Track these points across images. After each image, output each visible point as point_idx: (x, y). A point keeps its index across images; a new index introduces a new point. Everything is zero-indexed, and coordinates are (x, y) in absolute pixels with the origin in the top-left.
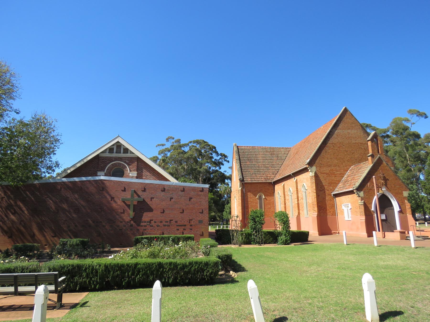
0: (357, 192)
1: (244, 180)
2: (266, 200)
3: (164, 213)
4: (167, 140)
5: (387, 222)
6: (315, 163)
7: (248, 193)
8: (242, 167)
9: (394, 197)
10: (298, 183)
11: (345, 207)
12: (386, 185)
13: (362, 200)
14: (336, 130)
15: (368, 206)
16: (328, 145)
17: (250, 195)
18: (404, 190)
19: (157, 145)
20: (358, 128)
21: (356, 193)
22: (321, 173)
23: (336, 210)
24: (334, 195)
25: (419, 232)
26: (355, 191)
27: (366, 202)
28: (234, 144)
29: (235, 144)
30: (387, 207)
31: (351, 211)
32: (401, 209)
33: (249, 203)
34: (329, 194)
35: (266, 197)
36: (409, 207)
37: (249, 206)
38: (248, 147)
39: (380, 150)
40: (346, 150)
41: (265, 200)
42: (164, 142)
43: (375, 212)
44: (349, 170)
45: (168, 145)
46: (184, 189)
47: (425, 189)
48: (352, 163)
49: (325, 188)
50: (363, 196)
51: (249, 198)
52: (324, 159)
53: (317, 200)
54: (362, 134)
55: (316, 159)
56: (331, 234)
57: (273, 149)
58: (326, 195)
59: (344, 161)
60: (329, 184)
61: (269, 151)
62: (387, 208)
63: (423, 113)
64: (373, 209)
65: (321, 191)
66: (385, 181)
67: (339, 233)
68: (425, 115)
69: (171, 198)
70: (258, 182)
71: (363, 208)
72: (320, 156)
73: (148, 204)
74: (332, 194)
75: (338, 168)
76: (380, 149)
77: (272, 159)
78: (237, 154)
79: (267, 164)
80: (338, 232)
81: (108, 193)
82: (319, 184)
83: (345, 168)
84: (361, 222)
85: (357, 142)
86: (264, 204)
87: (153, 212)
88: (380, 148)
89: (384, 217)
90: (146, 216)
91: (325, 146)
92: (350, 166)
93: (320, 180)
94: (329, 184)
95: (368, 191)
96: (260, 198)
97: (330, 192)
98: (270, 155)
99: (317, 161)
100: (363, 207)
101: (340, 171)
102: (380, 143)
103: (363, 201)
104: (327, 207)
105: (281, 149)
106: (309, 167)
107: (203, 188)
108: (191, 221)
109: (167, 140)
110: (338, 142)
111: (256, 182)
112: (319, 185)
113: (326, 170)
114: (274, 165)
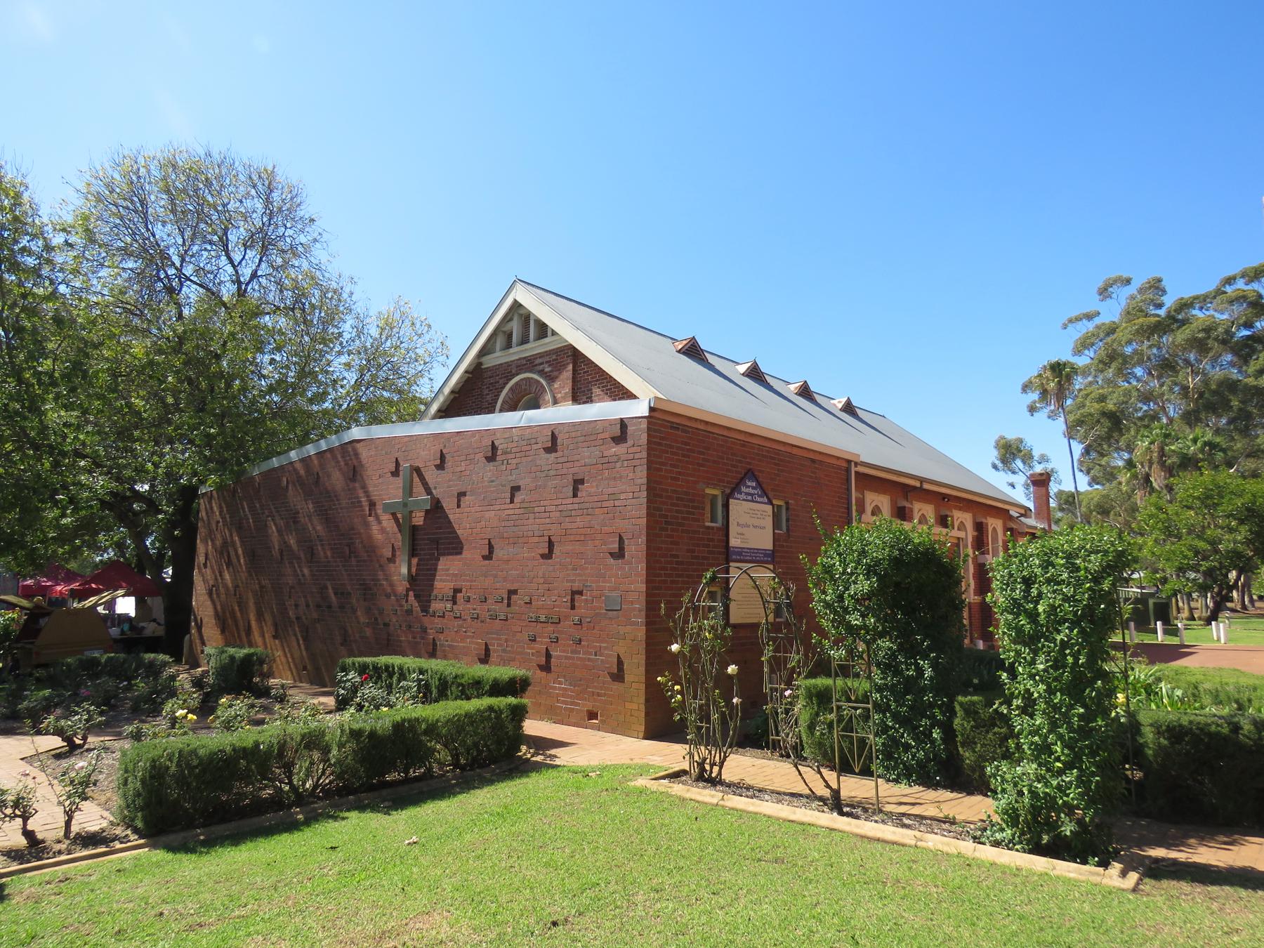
3: (491, 559)
4: (1100, 294)
19: (1065, 320)
42: (1093, 303)
45: (1111, 312)
46: (554, 437)
69: (515, 489)
73: (450, 522)
81: (364, 487)
87: (463, 556)
90: (448, 571)
107: (623, 423)
108: (577, 597)
109: (1104, 292)
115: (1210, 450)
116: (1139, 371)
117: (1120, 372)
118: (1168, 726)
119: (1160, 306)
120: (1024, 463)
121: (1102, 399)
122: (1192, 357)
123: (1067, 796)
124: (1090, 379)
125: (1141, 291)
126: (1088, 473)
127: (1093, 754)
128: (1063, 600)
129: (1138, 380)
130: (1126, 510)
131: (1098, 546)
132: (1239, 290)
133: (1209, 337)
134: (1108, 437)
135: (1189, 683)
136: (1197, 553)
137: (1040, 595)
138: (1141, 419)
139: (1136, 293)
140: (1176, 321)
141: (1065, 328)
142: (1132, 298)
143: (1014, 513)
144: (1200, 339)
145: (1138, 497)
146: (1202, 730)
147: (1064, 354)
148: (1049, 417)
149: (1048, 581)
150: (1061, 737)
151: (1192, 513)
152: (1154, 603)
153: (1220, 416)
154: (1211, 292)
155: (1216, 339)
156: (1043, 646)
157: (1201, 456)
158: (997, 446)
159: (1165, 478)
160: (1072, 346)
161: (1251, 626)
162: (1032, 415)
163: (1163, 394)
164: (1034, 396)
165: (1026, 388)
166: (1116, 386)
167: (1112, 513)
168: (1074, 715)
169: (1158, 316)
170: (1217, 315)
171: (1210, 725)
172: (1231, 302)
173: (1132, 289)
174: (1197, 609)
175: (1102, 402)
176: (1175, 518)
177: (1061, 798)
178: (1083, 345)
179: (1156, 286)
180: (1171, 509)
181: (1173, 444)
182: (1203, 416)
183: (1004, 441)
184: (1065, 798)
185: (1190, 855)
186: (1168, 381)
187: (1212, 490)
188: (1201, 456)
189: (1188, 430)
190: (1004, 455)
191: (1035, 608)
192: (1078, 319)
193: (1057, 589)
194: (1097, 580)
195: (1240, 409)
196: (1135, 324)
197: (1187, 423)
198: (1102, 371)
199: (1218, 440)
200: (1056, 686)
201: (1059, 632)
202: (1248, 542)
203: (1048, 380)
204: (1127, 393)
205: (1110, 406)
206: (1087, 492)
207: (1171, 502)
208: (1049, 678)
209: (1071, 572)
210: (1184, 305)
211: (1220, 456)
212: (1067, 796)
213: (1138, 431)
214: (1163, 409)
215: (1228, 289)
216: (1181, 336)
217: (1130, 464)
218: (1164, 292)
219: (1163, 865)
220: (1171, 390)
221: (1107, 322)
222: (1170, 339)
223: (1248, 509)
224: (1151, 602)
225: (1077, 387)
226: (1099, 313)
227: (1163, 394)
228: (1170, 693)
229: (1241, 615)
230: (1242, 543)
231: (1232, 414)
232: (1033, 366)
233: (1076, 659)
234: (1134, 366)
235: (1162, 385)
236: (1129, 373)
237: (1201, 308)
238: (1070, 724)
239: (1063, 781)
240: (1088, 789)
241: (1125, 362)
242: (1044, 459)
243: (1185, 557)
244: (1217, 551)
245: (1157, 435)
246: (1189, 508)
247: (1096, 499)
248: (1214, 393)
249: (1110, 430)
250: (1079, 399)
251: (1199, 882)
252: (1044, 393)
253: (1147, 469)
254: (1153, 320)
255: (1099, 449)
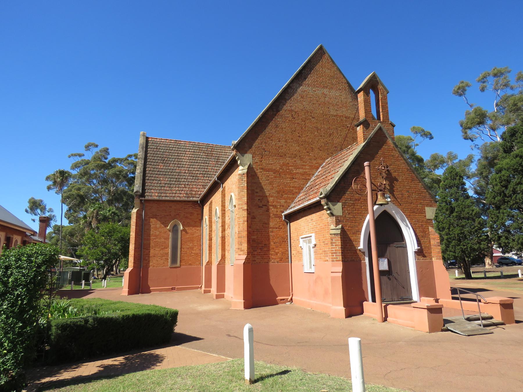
0: (327, 204)
1: (146, 194)
2: (186, 232)
4: (86, 148)
5: (391, 277)
6: (250, 147)
7: (152, 220)
8: (147, 172)
9: (407, 218)
10: (226, 195)
11: (304, 241)
12: (392, 191)
13: (337, 224)
14: (301, 85)
15: (352, 238)
16: (282, 112)
17: (155, 224)
18: (427, 206)
19: (70, 154)
20: (342, 88)
21: (325, 207)
22: (262, 169)
23: (289, 249)
24: (287, 216)
25: (458, 301)
26: (323, 202)
27: (346, 228)
28: (141, 133)
29: (144, 133)
30: (393, 242)
31: (315, 252)
32: (421, 247)
33: (152, 238)
34: (277, 215)
35: (186, 228)
36: (438, 243)
37: (152, 244)
38: (167, 141)
39: (381, 114)
40: (317, 128)
41: (184, 232)
42: (82, 151)
43: (367, 253)
44: (321, 167)
45: (89, 156)
47: (437, 222)
48: (328, 154)
49: (268, 202)
50: (340, 214)
51: (152, 230)
52: (272, 140)
53: (249, 227)
54: (350, 100)
55: (254, 140)
56: (275, 303)
57: (212, 147)
58: (270, 217)
59: (312, 148)
60: (278, 192)
61: (204, 149)
62: (391, 245)
63: (428, 133)
64: (361, 246)
65: (259, 207)
66: (390, 182)
67: (292, 299)
68: (431, 135)
70: (172, 199)
71: (339, 243)
72: (264, 133)
74: (283, 214)
75: (299, 162)
76: (382, 111)
77: (208, 162)
78: (143, 148)
79: (195, 169)
80: (290, 298)
82: (257, 192)
83: (314, 162)
84: (333, 278)
85: (339, 113)
86: (181, 240)
88: (382, 109)
89: (384, 265)
91: (275, 115)
92: (324, 160)
93: (260, 183)
94: (278, 192)
95: (352, 202)
96: (175, 229)
97: (279, 210)
98: (205, 157)
99: (256, 143)
100: (338, 242)
101: (302, 168)
102: (382, 98)
103: (340, 226)
104: (270, 243)
105: (227, 149)
106: (238, 154)
109: (88, 147)
110: (302, 110)
111: (168, 198)
112: (256, 194)
113: (275, 163)
114: (209, 173)
115: (114, 215)
116: (95, 181)
117: (88, 180)
118: (62, 325)
119: (106, 159)
120: (41, 211)
121: (79, 189)
122: (114, 180)
123: (6, 365)
124: (76, 180)
125: (100, 151)
126: (68, 218)
127: (22, 342)
128: (22, 276)
129: (94, 185)
130: (80, 235)
131: (44, 252)
132: (132, 160)
133: (120, 174)
134: (78, 205)
135: (80, 306)
136: (102, 253)
137: (11, 274)
138: (93, 200)
139: (99, 151)
140: (111, 165)
141: (70, 157)
142: (97, 153)
143: (28, 233)
144: (117, 174)
145: (86, 230)
146: (74, 324)
147: (67, 168)
148: (56, 193)
149: (17, 267)
150: (8, 338)
151: (103, 238)
152: (84, 273)
153: (119, 203)
154: (124, 158)
155: (122, 175)
156: (8, 297)
157: (110, 217)
158: (30, 202)
159: (97, 224)
160: (71, 165)
161: (117, 280)
162: (49, 191)
163: (102, 192)
164: (50, 183)
165: (48, 178)
166: (85, 185)
167: (75, 236)
168: (17, 327)
169: (105, 162)
170: (124, 167)
171: (78, 322)
172: (129, 164)
173: (98, 150)
174: (100, 275)
175: (79, 190)
176: (97, 239)
177: (3, 367)
178: (75, 166)
179: (106, 151)
180: (96, 236)
181: (102, 211)
182: (114, 202)
183: (34, 200)
184: (5, 367)
185: (59, 377)
186: (104, 187)
187: (111, 230)
188: (110, 217)
189: (108, 207)
190: (32, 206)
191: (8, 280)
192: (75, 155)
193: (20, 271)
194: (39, 267)
195: (126, 202)
196: (96, 163)
197: (108, 204)
198: (81, 178)
199: (117, 212)
200: (10, 315)
201: (17, 290)
202: (120, 249)
203: (58, 177)
204: (89, 189)
205: (82, 193)
206: (67, 226)
207: (97, 233)
208: (8, 312)
209: (29, 263)
210: (115, 161)
211: (116, 218)
212: (6, 365)
213: (90, 204)
214: (101, 197)
215: (129, 159)
216: (112, 171)
217: (85, 217)
218: (109, 154)
219: (46, 385)
220: (105, 191)
221: (86, 159)
222: (108, 172)
223: (122, 238)
224: (83, 272)
225: (70, 183)
226: (84, 155)
227: (102, 192)
228: (72, 310)
229: (115, 276)
230: (118, 250)
231: (123, 203)
232: (52, 171)
233: (22, 302)
234: (93, 179)
235: (102, 188)
236: (91, 181)
237: (120, 163)
238: (14, 332)
239: (5, 359)
240: (17, 360)
241: (90, 177)
242: (51, 210)
243: (98, 255)
244: (109, 253)
245: (97, 207)
246: (103, 236)
247: (69, 230)
248: (119, 194)
249: (80, 202)
250: (70, 188)
251: (57, 388)
252: (55, 183)
253: (91, 220)
254: (103, 163)
255: (74, 209)
